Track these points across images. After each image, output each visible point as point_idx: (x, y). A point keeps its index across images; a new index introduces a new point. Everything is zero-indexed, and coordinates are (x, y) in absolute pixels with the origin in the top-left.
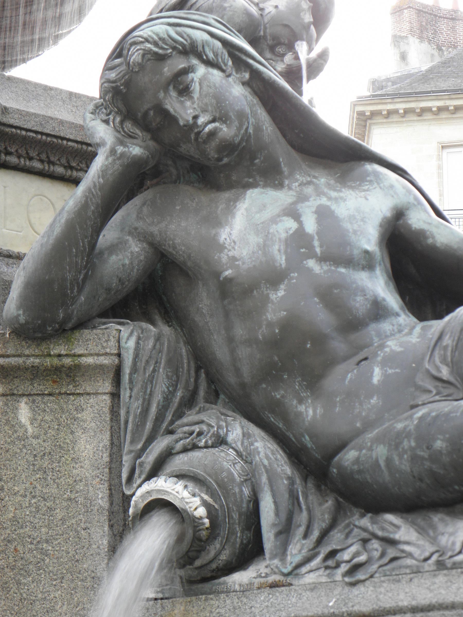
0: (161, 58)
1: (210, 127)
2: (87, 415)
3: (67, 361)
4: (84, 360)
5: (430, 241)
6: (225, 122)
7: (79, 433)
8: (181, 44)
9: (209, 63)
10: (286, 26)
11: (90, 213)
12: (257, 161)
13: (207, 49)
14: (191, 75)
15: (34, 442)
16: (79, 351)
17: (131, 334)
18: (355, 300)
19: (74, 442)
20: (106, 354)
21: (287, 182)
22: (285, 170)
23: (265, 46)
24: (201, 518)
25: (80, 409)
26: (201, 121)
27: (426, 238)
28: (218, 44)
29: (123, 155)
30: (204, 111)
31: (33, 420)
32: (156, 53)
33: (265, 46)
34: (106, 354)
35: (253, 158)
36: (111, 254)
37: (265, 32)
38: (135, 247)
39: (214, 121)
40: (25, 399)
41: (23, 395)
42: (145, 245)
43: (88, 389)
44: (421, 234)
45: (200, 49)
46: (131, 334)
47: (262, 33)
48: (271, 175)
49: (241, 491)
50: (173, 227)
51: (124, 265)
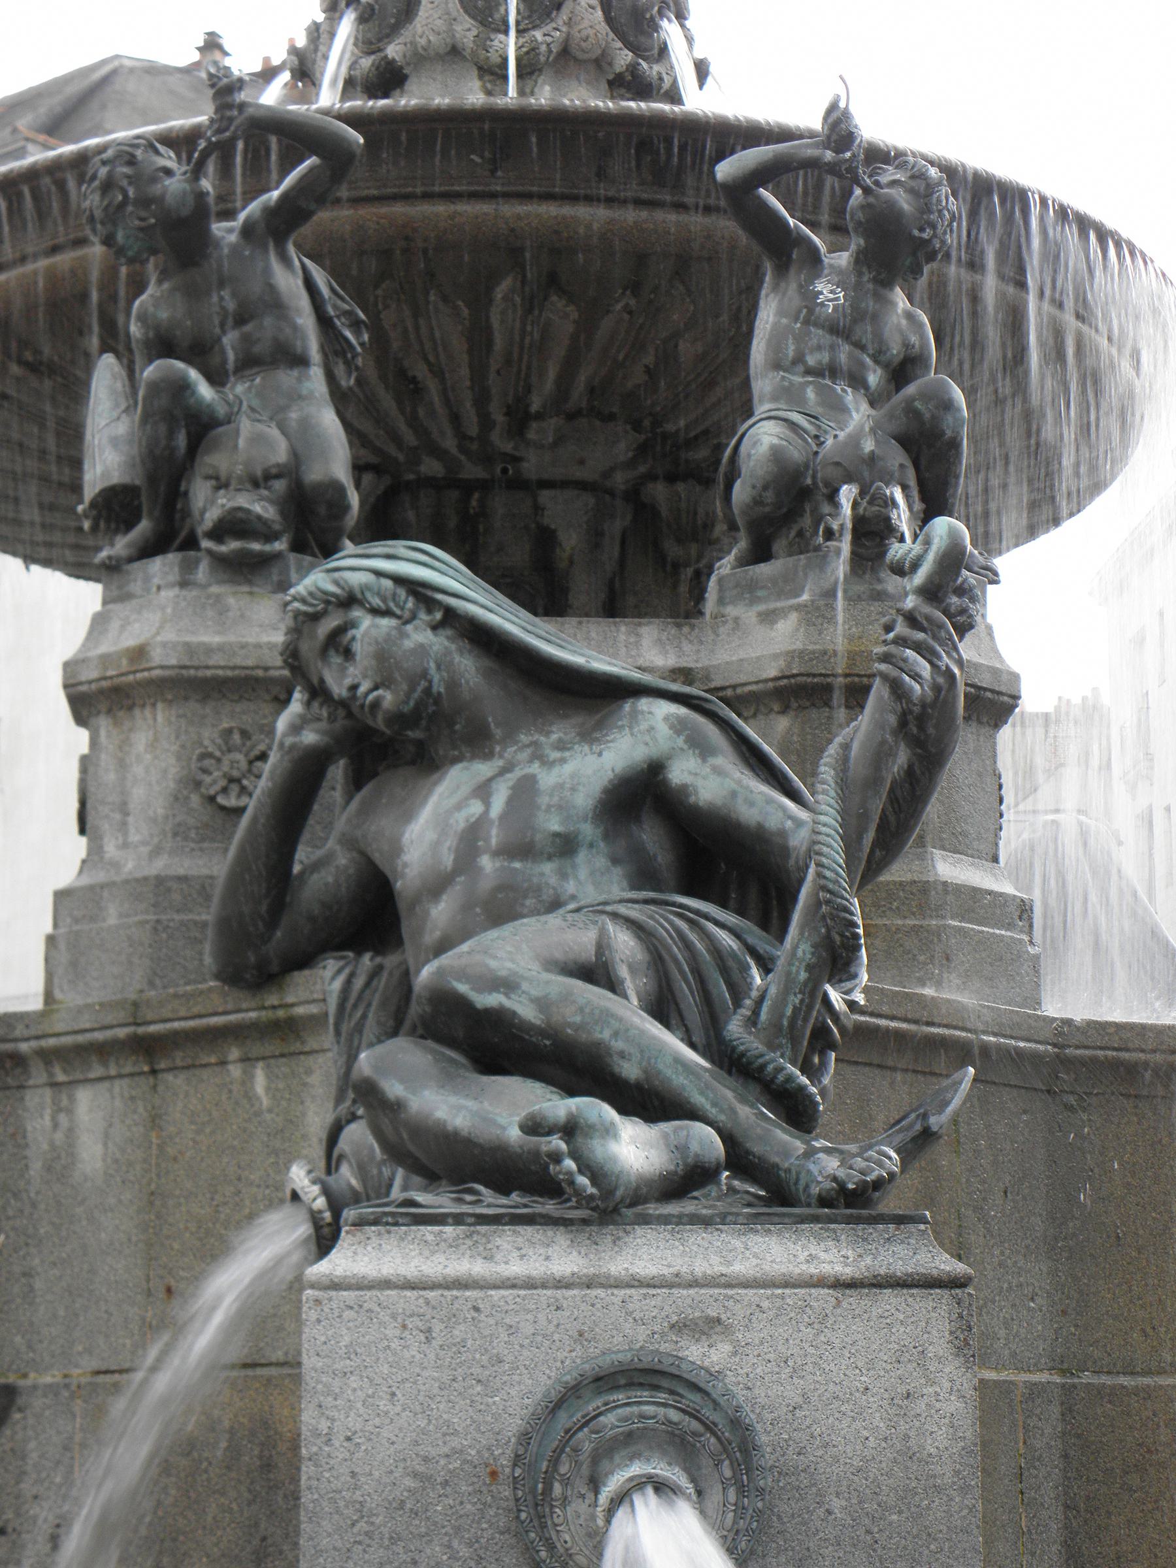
0: (315, 617)
1: (371, 697)
2: (315, 1079)
3: (281, 1013)
4: (300, 1010)
5: (692, 799)
6: (388, 687)
7: (308, 1103)
8: (333, 595)
9: (376, 612)
10: (838, 464)
11: (260, 827)
12: (457, 727)
13: (368, 595)
14: (350, 633)
15: (268, 1117)
16: (290, 999)
17: (339, 971)
18: (523, 905)
19: (304, 1114)
20: (314, 1001)
21: (498, 749)
22: (498, 732)
23: (820, 498)
24: (320, 1212)
25: (309, 1072)
26: (362, 689)
27: (687, 795)
28: (387, 584)
29: (293, 747)
30: (365, 677)
31: (268, 1089)
32: (306, 614)
33: (820, 498)
34: (314, 1001)
35: (451, 724)
36: (312, 873)
37: (814, 477)
38: (343, 859)
39: (376, 688)
40: (261, 1064)
41: (257, 1059)
42: (355, 854)
43: (316, 1046)
44: (684, 789)
45: (359, 596)
46: (339, 971)
47: (809, 481)
48: (476, 740)
49: (380, 1172)
50: (373, 828)
51: (326, 884)
